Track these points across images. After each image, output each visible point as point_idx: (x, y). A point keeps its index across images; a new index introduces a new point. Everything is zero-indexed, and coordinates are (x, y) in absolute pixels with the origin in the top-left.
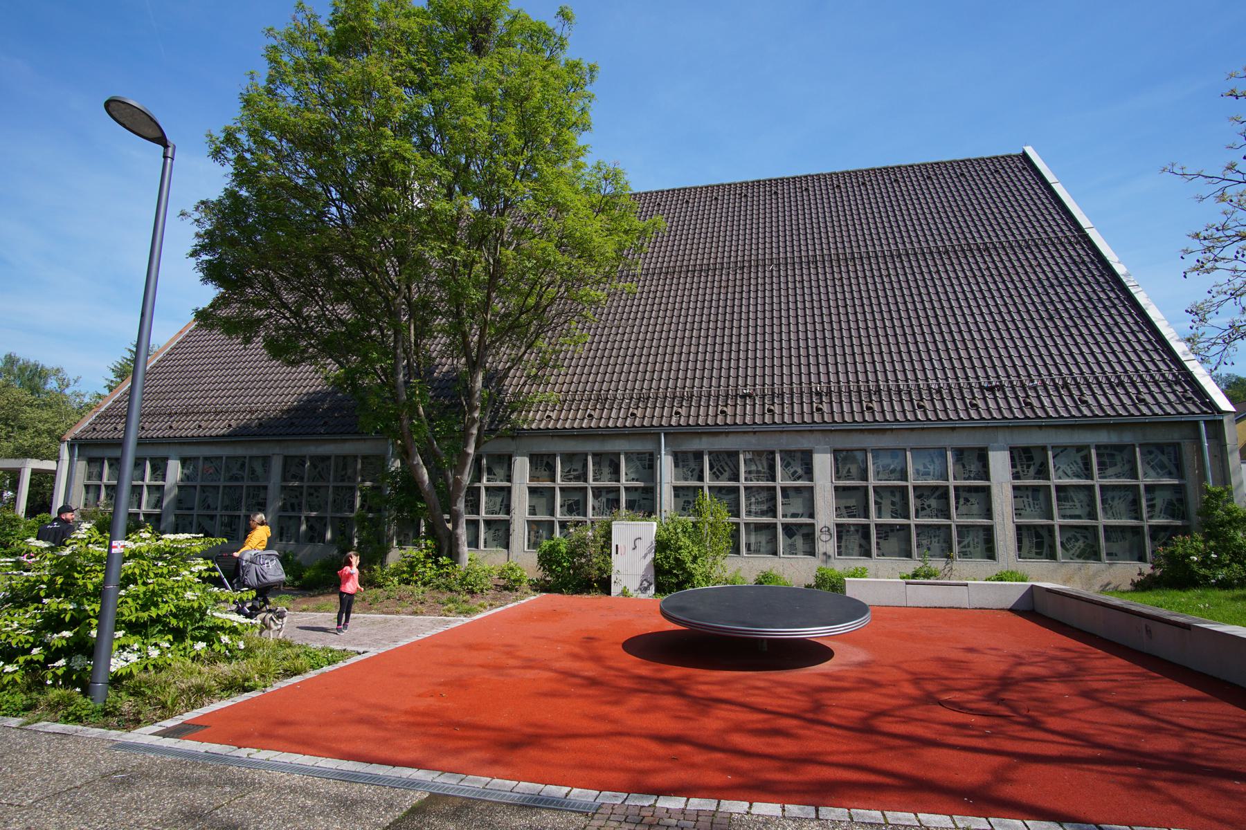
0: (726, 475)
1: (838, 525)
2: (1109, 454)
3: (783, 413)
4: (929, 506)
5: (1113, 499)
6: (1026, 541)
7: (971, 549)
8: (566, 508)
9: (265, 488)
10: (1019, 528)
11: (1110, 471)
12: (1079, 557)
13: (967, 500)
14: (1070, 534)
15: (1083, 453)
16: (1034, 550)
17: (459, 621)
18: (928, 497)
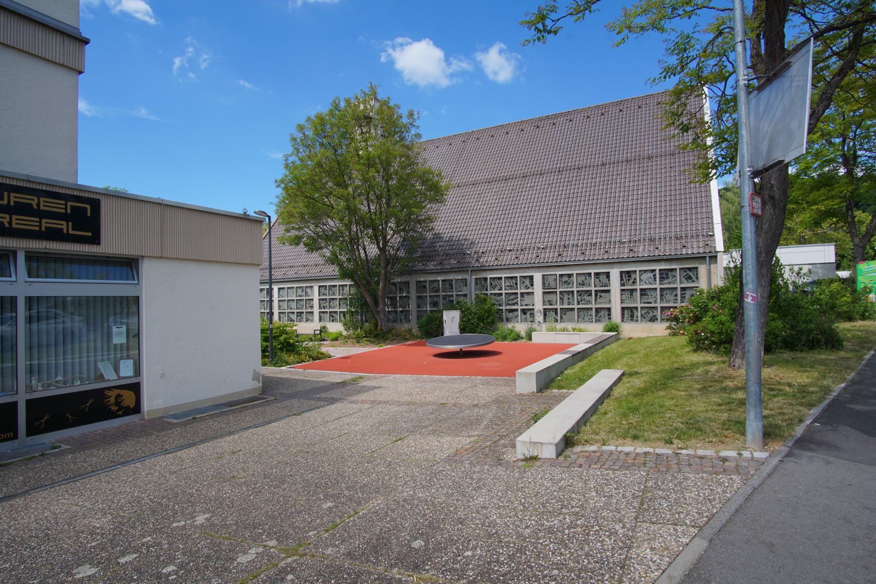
0: (498, 288)
1: (544, 309)
2: (665, 275)
3: (523, 259)
4: (584, 299)
5: (666, 294)
6: (626, 315)
7: (602, 318)
8: (432, 305)
9: (312, 300)
10: (623, 309)
11: (666, 281)
12: (649, 321)
13: (601, 296)
14: (645, 311)
15: (654, 273)
16: (630, 318)
17: (376, 348)
18: (584, 296)
